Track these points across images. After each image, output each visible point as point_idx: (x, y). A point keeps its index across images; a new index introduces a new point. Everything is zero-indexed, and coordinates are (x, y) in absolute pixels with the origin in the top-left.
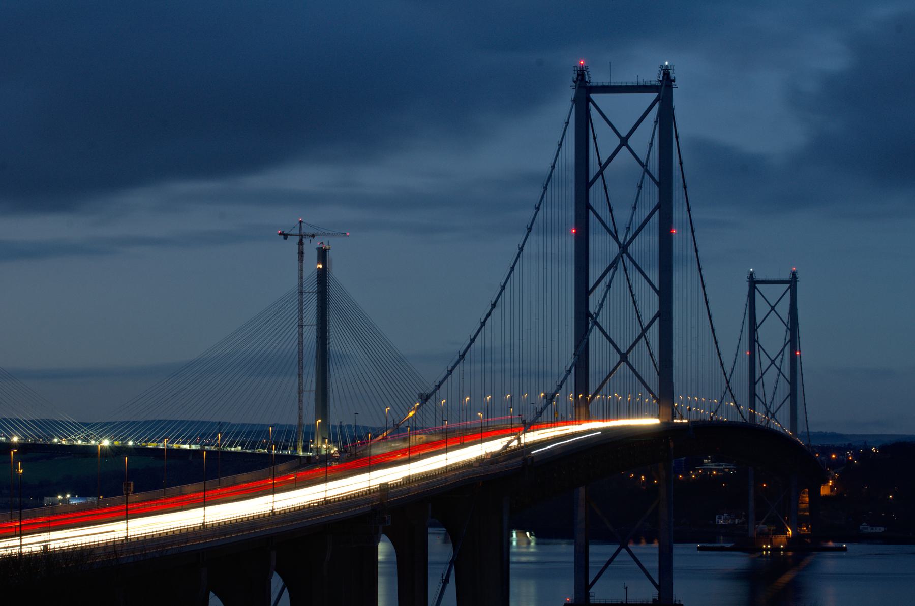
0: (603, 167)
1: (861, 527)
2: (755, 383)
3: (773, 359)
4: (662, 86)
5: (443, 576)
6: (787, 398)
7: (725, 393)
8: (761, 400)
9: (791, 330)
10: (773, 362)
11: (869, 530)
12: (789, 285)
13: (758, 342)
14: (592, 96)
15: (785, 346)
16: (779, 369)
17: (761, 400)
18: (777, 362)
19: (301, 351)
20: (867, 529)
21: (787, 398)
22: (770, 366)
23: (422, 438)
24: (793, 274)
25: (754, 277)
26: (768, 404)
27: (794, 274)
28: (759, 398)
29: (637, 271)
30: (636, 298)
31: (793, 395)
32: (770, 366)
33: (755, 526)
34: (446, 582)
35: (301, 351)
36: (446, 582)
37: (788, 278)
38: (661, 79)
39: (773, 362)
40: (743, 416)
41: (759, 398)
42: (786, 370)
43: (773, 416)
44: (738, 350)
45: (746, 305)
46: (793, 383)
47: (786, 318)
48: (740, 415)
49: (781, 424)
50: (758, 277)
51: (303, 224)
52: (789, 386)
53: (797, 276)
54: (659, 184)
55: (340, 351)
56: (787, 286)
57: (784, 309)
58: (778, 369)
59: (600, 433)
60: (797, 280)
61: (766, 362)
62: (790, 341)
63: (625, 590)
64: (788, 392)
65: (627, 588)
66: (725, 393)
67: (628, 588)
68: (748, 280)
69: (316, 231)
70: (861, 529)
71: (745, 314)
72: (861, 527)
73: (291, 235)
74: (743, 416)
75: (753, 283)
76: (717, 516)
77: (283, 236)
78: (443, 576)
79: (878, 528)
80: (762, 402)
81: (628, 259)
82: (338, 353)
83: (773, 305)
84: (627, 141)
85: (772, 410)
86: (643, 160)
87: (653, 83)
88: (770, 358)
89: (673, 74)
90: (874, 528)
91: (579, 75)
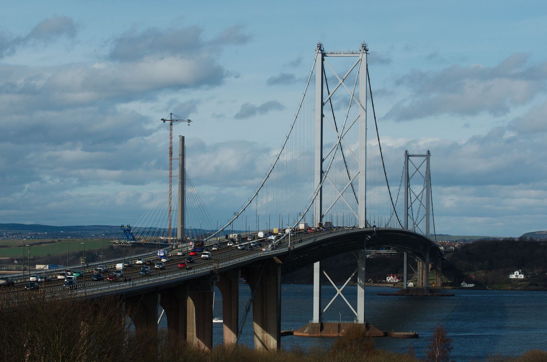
1: (462, 284)
2: (408, 209)
3: (417, 168)
5: (246, 308)
6: (424, 161)
10: (417, 197)
11: (466, 285)
16: (421, 202)
18: (420, 198)
19: (171, 148)
20: (465, 285)
21: (424, 161)
22: (416, 171)
23: (235, 236)
24: (428, 152)
26: (415, 220)
27: (428, 152)
28: (410, 216)
30: (348, 164)
31: (427, 215)
32: (416, 171)
33: (407, 283)
34: (248, 310)
36: (248, 310)
39: (417, 197)
40: (402, 227)
41: (410, 216)
42: (424, 202)
43: (417, 226)
46: (427, 209)
49: (421, 230)
50: (410, 153)
51: (172, 115)
52: (425, 210)
54: (426, 209)
55: (194, 192)
57: (423, 169)
61: (413, 197)
64: (425, 213)
69: (178, 119)
70: (462, 285)
72: (462, 284)
73: (167, 120)
74: (402, 227)
75: (408, 156)
76: (387, 278)
77: (163, 121)
78: (246, 308)
79: (471, 285)
80: (411, 190)
82: (192, 193)
85: (417, 223)
88: (416, 168)
90: (469, 285)
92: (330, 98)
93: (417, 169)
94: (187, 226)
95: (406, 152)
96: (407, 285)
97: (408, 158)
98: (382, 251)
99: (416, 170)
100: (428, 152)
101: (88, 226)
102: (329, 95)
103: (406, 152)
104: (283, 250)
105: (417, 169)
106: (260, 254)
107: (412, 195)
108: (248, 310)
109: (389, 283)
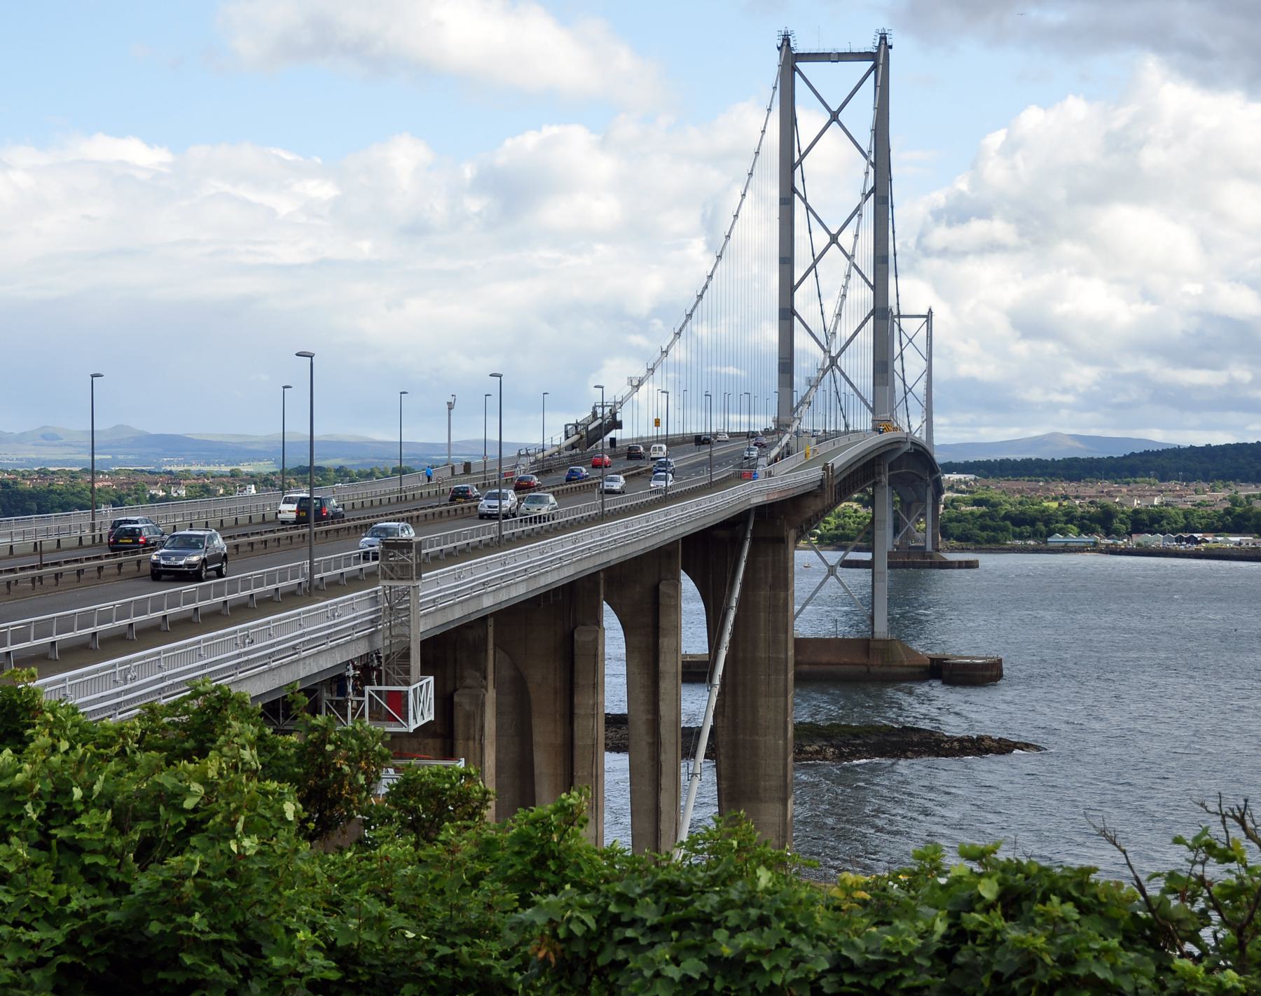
0: (802, 157)
7: (848, 276)
8: (863, 276)
9: (874, 165)
10: (834, 239)
17: (863, 276)
18: (846, 239)
19: (896, 276)
27: (883, 38)
35: (896, 276)
37: (871, 45)
45: (775, 88)
47: (866, 141)
50: (801, 45)
54: (874, 288)
56: (869, 64)
57: (861, 115)
58: (849, 257)
62: (874, 190)
66: (848, 276)
75: (791, 60)
83: (834, 109)
86: (849, 252)
95: (786, 39)
97: (795, 69)
99: (841, 117)
100: (883, 38)
103: (786, 39)
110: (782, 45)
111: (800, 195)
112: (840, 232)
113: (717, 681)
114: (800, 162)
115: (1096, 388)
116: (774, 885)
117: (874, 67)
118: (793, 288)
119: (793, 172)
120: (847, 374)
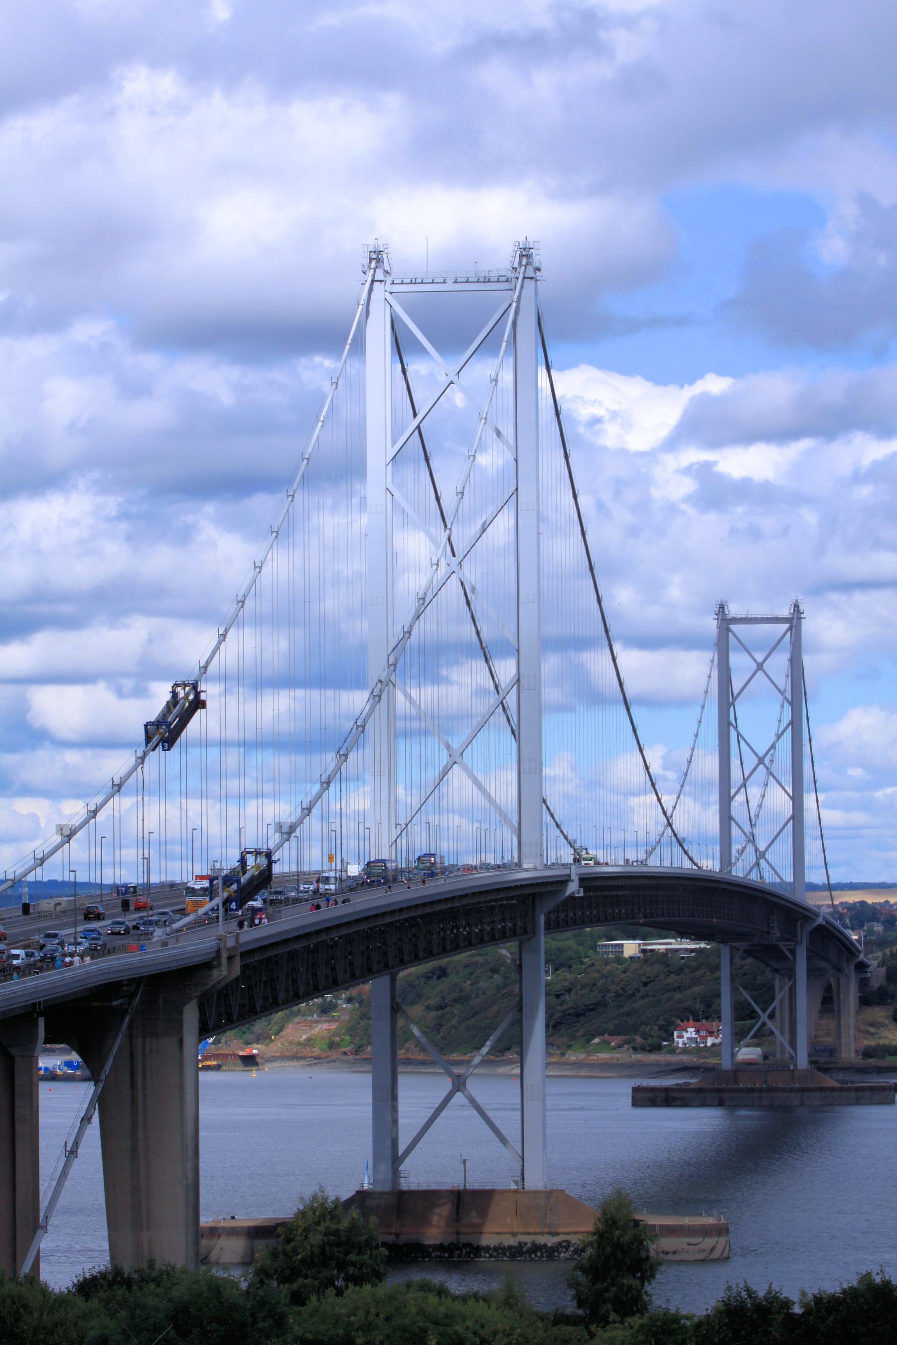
4: (793, 618)
12: (788, 625)
13: (736, 728)
14: (732, 627)
15: (779, 736)
18: (767, 761)
23: (60, 904)
25: (727, 612)
27: (796, 606)
29: (778, 785)
38: (792, 612)
44: (695, 740)
45: (713, 661)
48: (686, 857)
50: (734, 610)
53: (801, 608)
54: (792, 798)
57: (779, 663)
59: (178, 719)
60: (802, 616)
63: (463, 1165)
65: (465, 1161)
67: (467, 1163)
68: (716, 617)
71: (710, 677)
76: (676, 1033)
81: (788, 791)
84: (762, 666)
87: (785, 616)
89: (537, 257)
91: (720, 608)
92: (418, 427)
93: (760, 666)
94: (830, 882)
96: (733, 1055)
97: (729, 630)
98: (660, 944)
100: (796, 606)
101: (856, 883)
102: (415, 415)
104: (103, 962)
105: (760, 666)
106: (845, 931)
107: (475, 724)
108: (71, 1152)
109: (680, 1053)
110: (719, 612)
111: (733, 726)
112: (767, 849)
113: (57, 932)
114: (735, 863)
115: (878, 907)
116: (859, 1286)
117: (790, 629)
118: (731, 799)
119: (729, 711)
120: (776, 868)
